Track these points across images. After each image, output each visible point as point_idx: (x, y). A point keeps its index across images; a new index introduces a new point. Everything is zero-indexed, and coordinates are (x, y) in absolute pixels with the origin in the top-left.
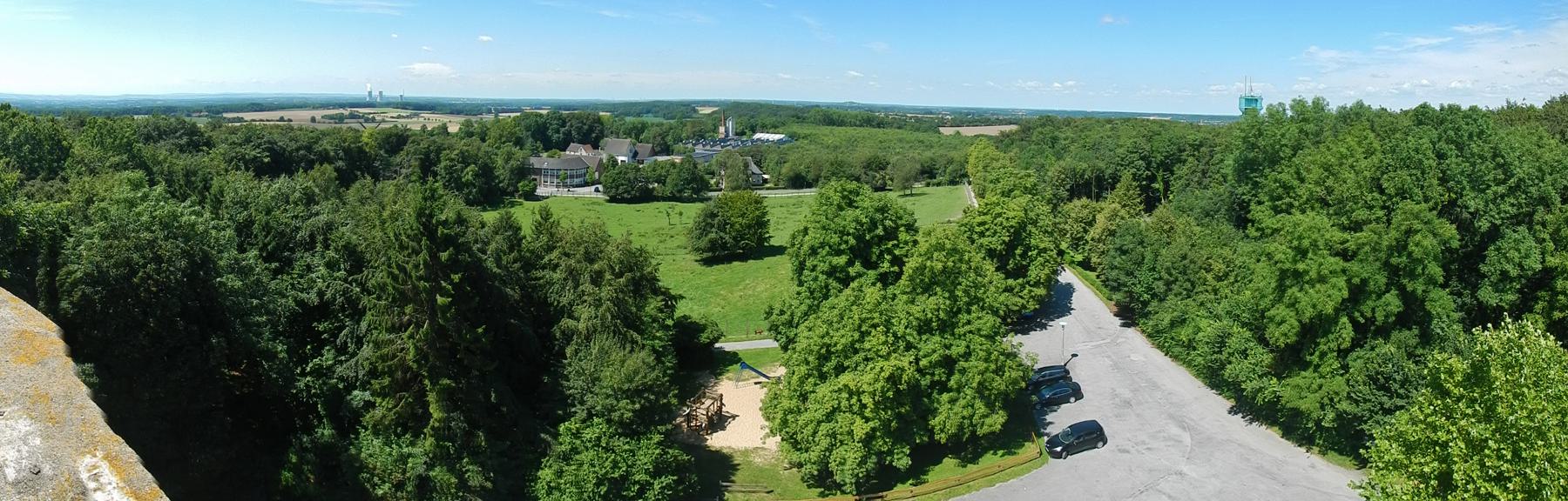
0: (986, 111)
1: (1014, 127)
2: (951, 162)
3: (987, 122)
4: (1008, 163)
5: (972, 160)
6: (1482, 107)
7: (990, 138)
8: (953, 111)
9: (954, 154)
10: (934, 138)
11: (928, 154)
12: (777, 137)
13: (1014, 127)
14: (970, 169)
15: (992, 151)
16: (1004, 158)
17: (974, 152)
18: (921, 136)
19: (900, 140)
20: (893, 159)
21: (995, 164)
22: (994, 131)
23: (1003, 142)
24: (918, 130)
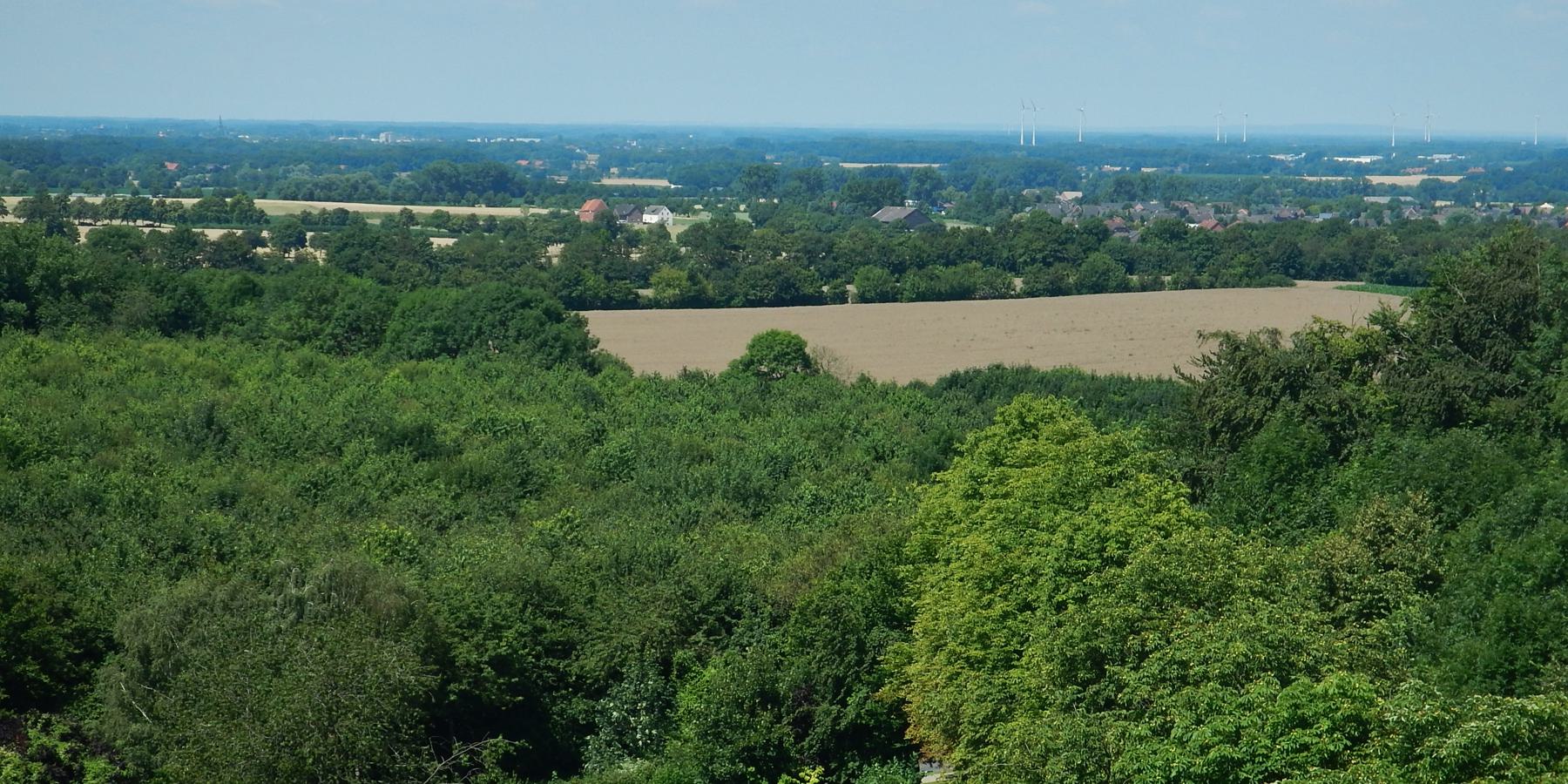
0: (1049, 165)
1: (1345, 308)
2: (716, 615)
3: (1069, 261)
4: (1301, 621)
5: (942, 602)
6: (881, 377)
7: (1106, 398)
8: (702, 170)
9: (765, 555)
10: (544, 409)
11: (487, 556)
12: (545, 212)
13: (1345, 308)
14: (923, 681)
15: (1155, 519)
16: (1274, 579)
17: (959, 530)
18: (396, 386)
19: (210, 433)
20: (148, 606)
21: (1194, 637)
22: (1159, 335)
23: (1255, 436)
24: (363, 333)
